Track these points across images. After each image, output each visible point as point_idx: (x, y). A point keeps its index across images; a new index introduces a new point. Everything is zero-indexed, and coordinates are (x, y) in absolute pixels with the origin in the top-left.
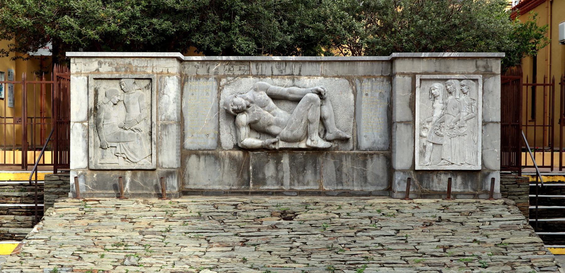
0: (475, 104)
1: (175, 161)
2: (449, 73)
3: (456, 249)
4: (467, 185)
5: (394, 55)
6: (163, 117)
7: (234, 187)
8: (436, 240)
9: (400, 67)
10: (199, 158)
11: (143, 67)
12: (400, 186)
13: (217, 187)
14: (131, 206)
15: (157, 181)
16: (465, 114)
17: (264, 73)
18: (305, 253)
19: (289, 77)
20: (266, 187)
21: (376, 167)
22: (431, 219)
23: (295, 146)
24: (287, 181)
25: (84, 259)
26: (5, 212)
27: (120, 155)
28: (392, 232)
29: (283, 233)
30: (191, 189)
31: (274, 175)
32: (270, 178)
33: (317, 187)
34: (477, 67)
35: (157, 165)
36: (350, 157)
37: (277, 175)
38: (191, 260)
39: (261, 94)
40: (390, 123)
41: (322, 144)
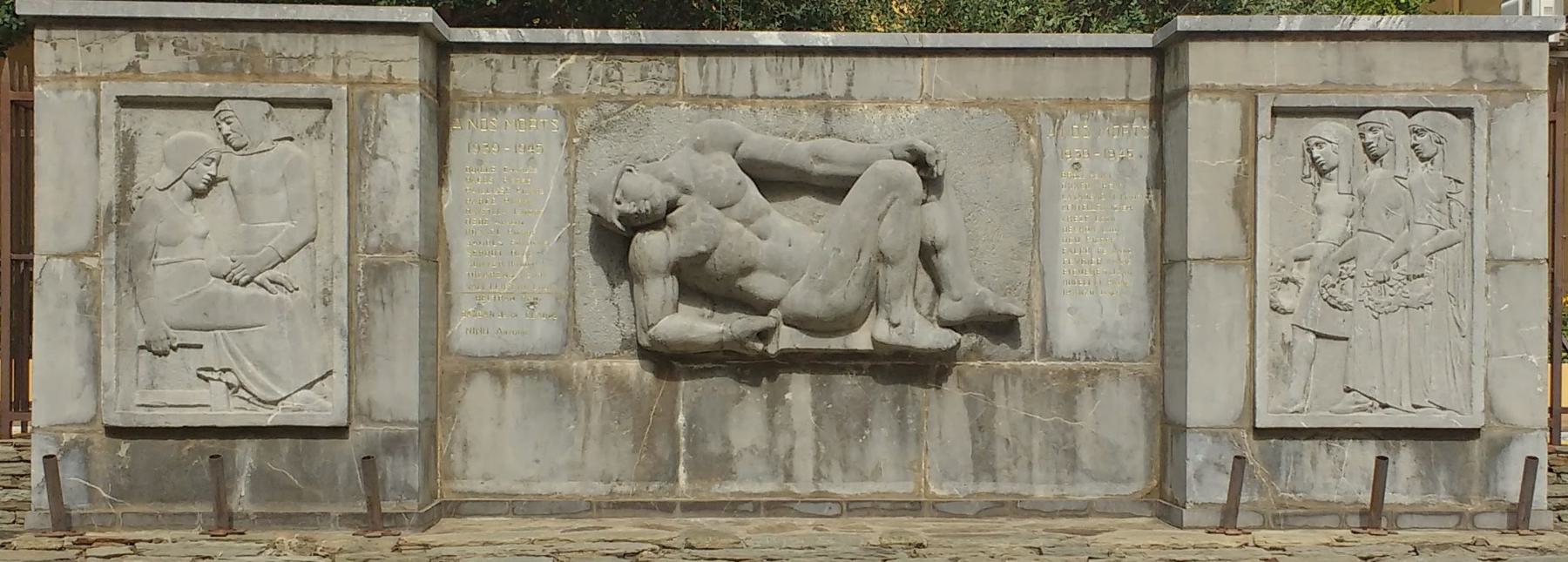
0: (1462, 197)
4: (1434, 480)
5: (1184, 22)
6: (374, 240)
7: (624, 488)
9: (1206, 64)
10: (503, 384)
11: (301, 59)
12: (1207, 488)
13: (564, 487)
15: (350, 469)
16: (1426, 230)
17: (725, 91)
19: (811, 102)
21: (1114, 419)
23: (835, 343)
24: (804, 467)
27: (215, 376)
30: (473, 493)
31: (765, 446)
32: (747, 455)
33: (909, 487)
34: (1468, 67)
36: (1019, 382)
37: (772, 444)
39: (719, 162)
40: (1166, 266)
41: (930, 337)
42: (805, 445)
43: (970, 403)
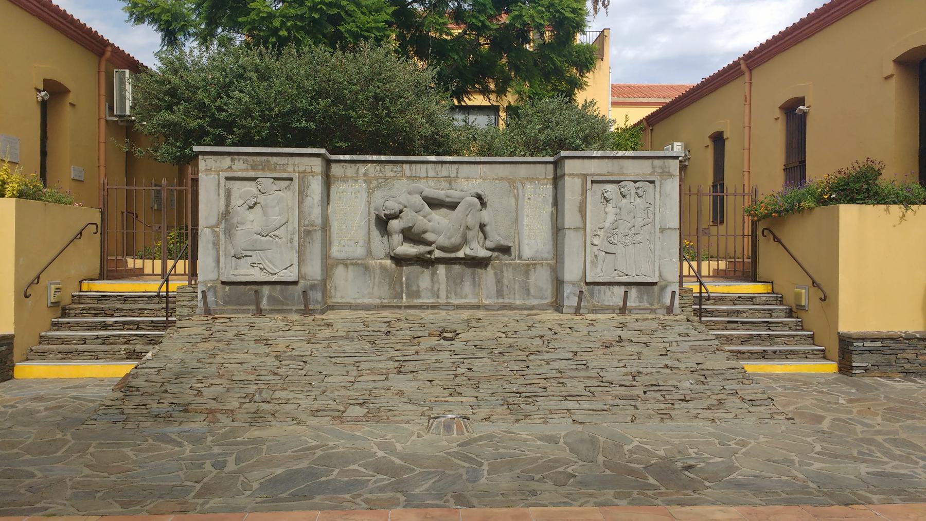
0: (652, 209)
1: (319, 272)
2: (623, 174)
3: (647, 377)
5: (563, 153)
6: (306, 223)
8: (622, 365)
9: (570, 166)
12: (571, 301)
13: (367, 301)
14: (268, 325)
16: (640, 219)
18: (472, 383)
20: (420, 301)
21: (541, 279)
22: (610, 338)
23: (453, 255)
24: (443, 294)
25: (204, 394)
26: (136, 327)
28: (570, 355)
29: (444, 356)
33: (477, 301)
34: (653, 167)
35: (301, 276)
37: (433, 287)
38: (336, 393)
40: (558, 231)
41: (483, 253)
42: (443, 287)
43: (496, 274)
